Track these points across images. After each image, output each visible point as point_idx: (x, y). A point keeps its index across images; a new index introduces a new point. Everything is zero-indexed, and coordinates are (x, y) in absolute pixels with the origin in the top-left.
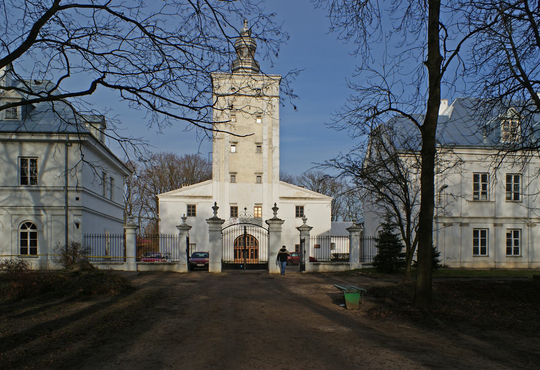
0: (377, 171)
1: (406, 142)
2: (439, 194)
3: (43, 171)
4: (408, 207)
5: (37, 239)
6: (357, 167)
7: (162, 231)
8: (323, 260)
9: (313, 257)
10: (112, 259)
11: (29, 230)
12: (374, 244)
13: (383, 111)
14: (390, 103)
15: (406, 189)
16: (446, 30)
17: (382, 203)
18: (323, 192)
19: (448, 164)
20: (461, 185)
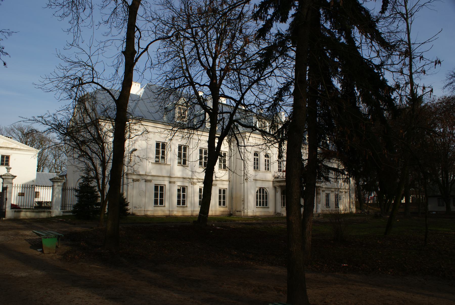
0: (79, 131)
1: (105, 111)
2: (130, 155)
4: (104, 164)
6: (62, 126)
8: (24, 207)
9: (15, 204)
12: (74, 194)
13: (87, 83)
14: (93, 78)
16: (140, 33)
17: (82, 159)
18: (31, 145)
19: (137, 132)
20: (146, 150)
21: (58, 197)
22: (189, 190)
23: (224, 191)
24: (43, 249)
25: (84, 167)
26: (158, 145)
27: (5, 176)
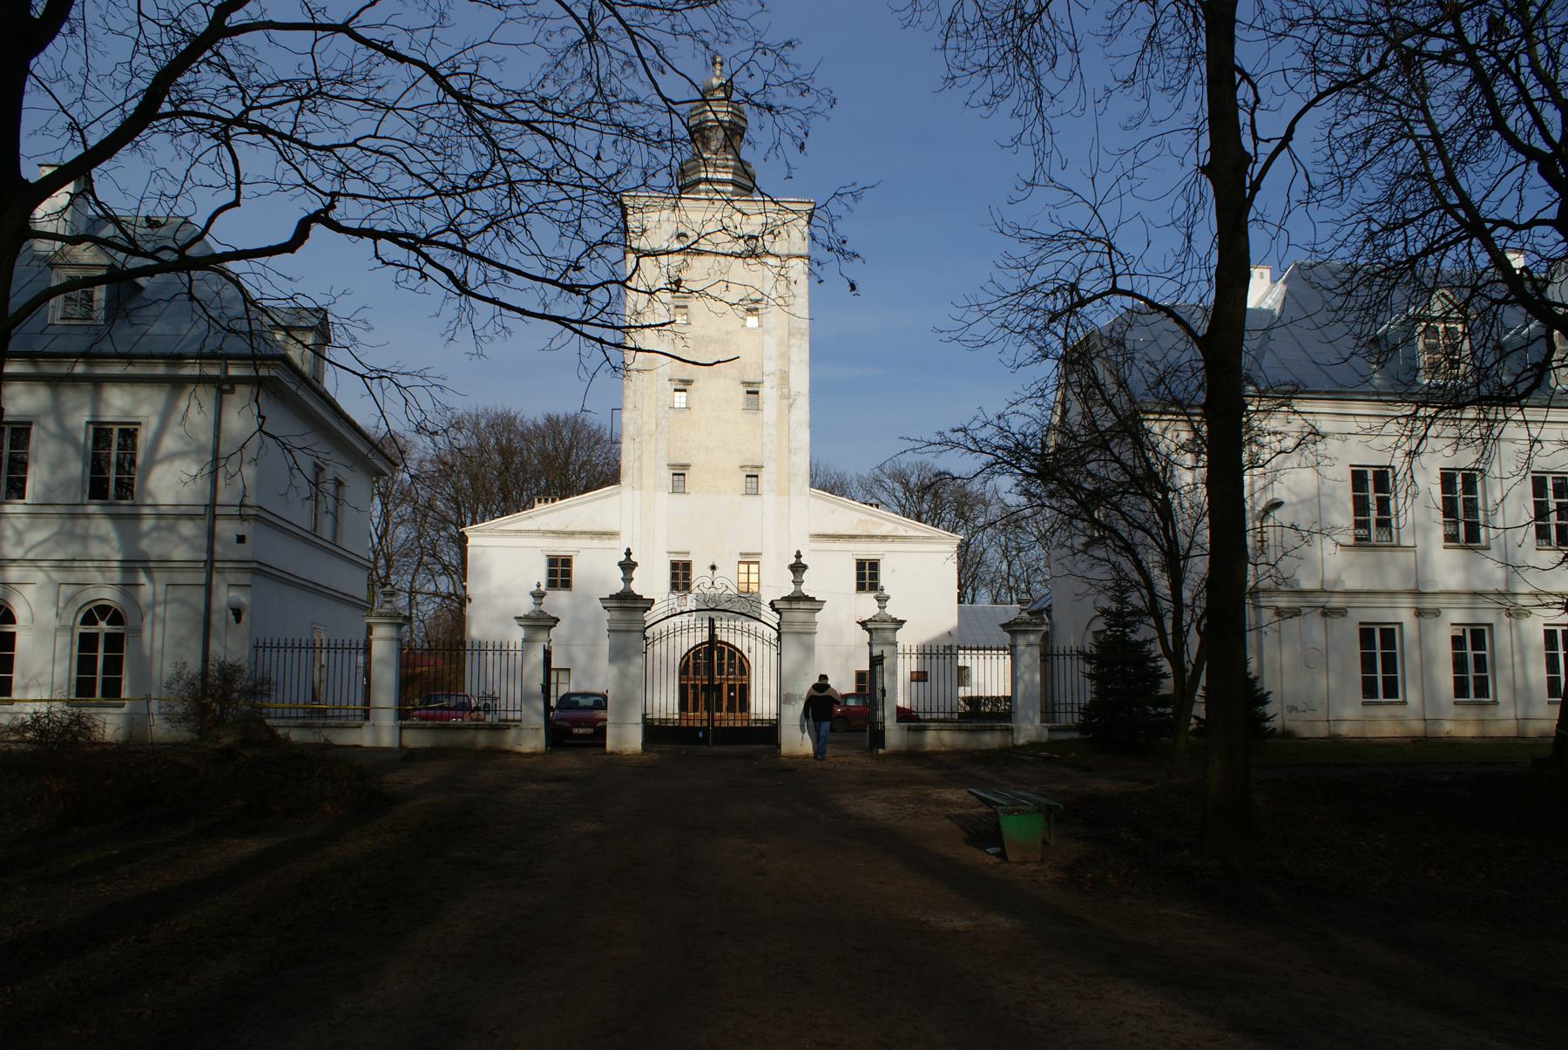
1: (1161, 380)
2: (1258, 524)
3: (151, 462)
4: (1174, 563)
5: (125, 654)
6: (1027, 449)
7: (479, 626)
8: (935, 716)
9: (907, 706)
10: (329, 713)
11: (103, 626)
12: (1081, 669)
13: (1096, 297)
14: (1114, 276)
16: (1254, 87)
17: (1100, 553)
18: (933, 521)
19: (1279, 441)
20: (1317, 500)
21: (1032, 680)
22: (1503, 638)
26: (1358, 477)
27: (875, 621)
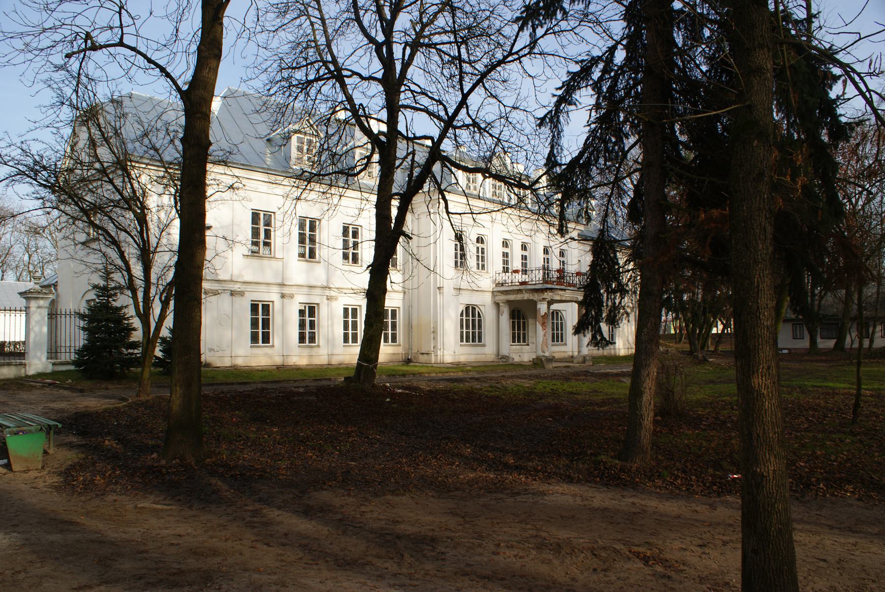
1: (146, 135)
4: (146, 255)
15: (142, 220)
22: (323, 313)
23: (355, 311)
24: (9, 461)
25: (100, 262)
